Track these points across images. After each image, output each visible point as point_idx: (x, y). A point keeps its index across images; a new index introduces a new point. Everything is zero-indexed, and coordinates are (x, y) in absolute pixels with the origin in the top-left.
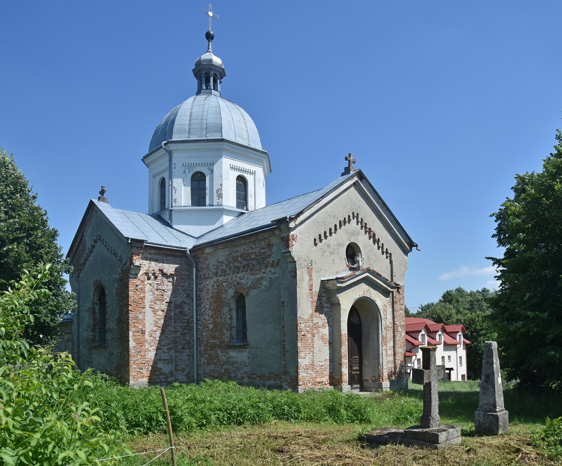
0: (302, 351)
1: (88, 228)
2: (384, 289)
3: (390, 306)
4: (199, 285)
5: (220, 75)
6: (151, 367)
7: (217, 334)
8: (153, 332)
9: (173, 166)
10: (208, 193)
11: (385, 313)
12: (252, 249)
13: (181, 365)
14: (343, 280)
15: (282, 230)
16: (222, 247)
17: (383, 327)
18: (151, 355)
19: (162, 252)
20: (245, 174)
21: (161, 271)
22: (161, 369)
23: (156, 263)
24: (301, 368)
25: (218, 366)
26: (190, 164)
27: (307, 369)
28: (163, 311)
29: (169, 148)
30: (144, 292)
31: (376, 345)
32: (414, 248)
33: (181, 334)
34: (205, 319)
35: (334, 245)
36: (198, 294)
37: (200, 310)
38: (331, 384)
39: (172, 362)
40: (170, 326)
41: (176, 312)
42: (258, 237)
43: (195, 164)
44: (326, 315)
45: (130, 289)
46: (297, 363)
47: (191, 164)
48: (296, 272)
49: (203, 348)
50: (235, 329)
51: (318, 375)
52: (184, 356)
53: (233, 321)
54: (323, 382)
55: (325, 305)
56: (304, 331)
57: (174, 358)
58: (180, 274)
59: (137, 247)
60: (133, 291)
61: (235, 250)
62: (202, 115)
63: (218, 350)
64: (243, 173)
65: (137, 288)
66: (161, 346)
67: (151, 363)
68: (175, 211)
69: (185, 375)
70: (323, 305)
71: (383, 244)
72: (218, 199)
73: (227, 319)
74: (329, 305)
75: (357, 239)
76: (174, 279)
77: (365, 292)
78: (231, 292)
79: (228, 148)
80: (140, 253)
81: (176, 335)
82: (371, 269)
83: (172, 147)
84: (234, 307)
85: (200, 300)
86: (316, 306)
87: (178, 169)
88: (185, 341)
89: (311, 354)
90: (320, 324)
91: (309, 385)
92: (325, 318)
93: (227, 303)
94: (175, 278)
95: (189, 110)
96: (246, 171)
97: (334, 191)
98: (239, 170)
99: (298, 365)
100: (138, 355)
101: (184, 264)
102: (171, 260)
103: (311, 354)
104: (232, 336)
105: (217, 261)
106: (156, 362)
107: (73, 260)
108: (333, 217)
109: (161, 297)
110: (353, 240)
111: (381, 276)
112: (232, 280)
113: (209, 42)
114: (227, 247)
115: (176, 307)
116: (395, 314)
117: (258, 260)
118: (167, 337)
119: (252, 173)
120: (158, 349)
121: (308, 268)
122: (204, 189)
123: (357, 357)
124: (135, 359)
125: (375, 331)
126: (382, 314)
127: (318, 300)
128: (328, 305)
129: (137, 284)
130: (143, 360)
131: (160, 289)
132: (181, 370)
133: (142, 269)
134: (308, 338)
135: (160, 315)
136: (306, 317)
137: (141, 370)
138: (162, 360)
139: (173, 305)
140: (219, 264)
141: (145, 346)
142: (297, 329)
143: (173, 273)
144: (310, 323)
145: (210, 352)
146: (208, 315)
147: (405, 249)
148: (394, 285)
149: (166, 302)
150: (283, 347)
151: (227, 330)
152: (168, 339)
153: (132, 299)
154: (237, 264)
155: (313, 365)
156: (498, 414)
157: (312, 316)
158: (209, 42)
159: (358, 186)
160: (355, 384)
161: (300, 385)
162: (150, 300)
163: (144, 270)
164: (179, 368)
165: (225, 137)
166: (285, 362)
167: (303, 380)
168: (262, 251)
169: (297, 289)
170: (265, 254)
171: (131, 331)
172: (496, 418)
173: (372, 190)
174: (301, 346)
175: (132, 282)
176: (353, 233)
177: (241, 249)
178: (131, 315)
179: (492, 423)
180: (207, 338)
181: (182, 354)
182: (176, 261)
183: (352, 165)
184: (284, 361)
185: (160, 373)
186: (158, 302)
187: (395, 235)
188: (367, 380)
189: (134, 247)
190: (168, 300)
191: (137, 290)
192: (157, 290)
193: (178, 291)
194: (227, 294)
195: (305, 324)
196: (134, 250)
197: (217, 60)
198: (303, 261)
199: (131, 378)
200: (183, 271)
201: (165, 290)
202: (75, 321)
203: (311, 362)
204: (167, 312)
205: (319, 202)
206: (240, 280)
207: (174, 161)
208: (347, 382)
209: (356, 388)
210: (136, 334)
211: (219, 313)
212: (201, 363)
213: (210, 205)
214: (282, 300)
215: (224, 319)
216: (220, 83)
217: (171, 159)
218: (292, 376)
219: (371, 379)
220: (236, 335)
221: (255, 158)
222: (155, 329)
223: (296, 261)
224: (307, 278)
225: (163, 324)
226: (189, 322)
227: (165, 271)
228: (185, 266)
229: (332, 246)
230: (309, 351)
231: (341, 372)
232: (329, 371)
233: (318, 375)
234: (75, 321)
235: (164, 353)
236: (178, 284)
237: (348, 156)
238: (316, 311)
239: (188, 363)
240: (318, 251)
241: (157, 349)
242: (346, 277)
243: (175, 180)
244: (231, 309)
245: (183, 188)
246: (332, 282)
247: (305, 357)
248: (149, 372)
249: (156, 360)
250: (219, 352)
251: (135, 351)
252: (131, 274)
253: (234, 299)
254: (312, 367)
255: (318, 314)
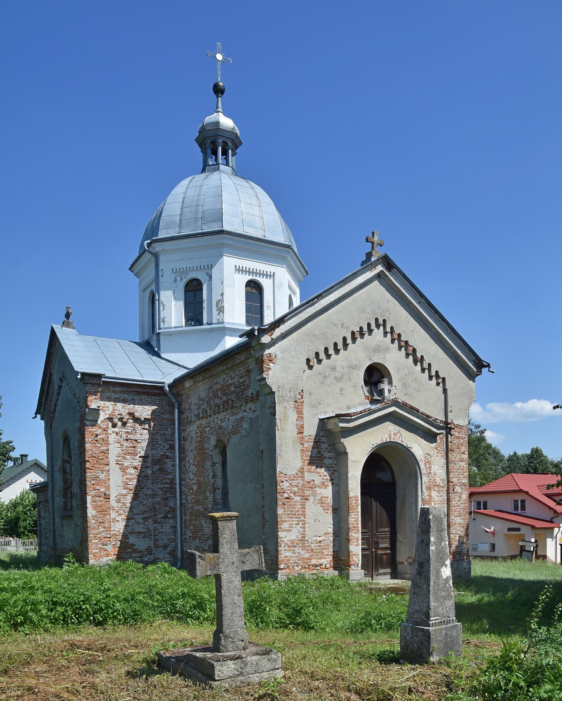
0: (285, 521)
1: (55, 364)
2: (426, 430)
3: (442, 456)
4: (183, 432)
5: (232, 143)
6: (119, 543)
7: (201, 497)
8: (122, 497)
9: (160, 274)
10: (206, 307)
11: (428, 466)
12: (232, 378)
13: (162, 540)
14: (350, 418)
15: (255, 348)
16: (201, 379)
17: (424, 486)
18: (119, 527)
19: (131, 390)
20: (260, 277)
21: (131, 414)
22: (134, 545)
23: (123, 404)
24: (283, 545)
25: (202, 541)
26: (181, 270)
27: (294, 546)
28: (135, 468)
29: (154, 249)
30: (106, 442)
31: (414, 513)
32: (485, 370)
33: (161, 498)
34: (189, 478)
35: (343, 367)
36: (182, 445)
37: (185, 466)
38: (335, 568)
39: (149, 535)
40: (146, 488)
41: (155, 469)
42: (235, 361)
43: (188, 269)
44: (328, 469)
45: (86, 440)
46: (276, 537)
47: (183, 268)
48: (275, 408)
49: (188, 517)
50: (221, 490)
51: (313, 555)
52: (167, 528)
53: (217, 480)
54: (321, 565)
55: (327, 455)
56: (289, 492)
57: (153, 531)
58: (159, 418)
59: (93, 384)
60: (91, 443)
61: (215, 381)
62: (198, 200)
63: (202, 520)
64: (256, 276)
65: (96, 439)
66: (133, 514)
67: (120, 537)
68: (164, 335)
69: (168, 553)
70: (323, 455)
71: (429, 365)
72: (219, 314)
73: (210, 477)
74: (333, 454)
75: (384, 358)
76: (150, 425)
77: (392, 434)
78: (213, 440)
79: (230, 242)
80: (97, 392)
81: (155, 500)
82: (399, 400)
83: (157, 247)
84: (218, 461)
85: (184, 452)
86: (311, 456)
87: (166, 278)
88: (168, 509)
89: (301, 525)
90: (317, 482)
91: (297, 569)
92: (326, 473)
93: (210, 455)
94: (152, 424)
95: (182, 195)
96: (260, 274)
97: (341, 287)
98: (249, 272)
99: (278, 540)
100: (100, 527)
101: (165, 405)
102: (146, 400)
103: (301, 525)
104: (216, 501)
105: (199, 398)
106: (127, 536)
107: (46, 406)
108: (340, 326)
109: (131, 450)
110: (377, 359)
111: (418, 411)
112: (214, 423)
113: (218, 97)
114: (206, 378)
115: (155, 462)
116: (450, 468)
117: (237, 393)
118: (142, 502)
119: (270, 276)
120: (128, 519)
121: (295, 401)
122: (201, 302)
123: (387, 529)
124: (96, 531)
125: (413, 492)
126: (422, 466)
127: (313, 448)
128: (331, 454)
129: (97, 433)
130: (107, 534)
131: (131, 440)
132: (162, 547)
133: (101, 413)
134: (296, 502)
135: (132, 474)
136: (292, 472)
137: (105, 547)
138: (136, 533)
139: (149, 460)
140: (201, 403)
141: (110, 515)
142: (277, 490)
143: (149, 417)
144: (299, 480)
145: (195, 522)
146: (192, 472)
147: (470, 371)
148: (441, 425)
149: (140, 457)
150: (263, 515)
151: (210, 492)
152: (143, 505)
153: (90, 453)
154: (217, 401)
155: (303, 540)
156: (430, 629)
157: (302, 470)
158: (218, 97)
159: (386, 279)
160: (382, 568)
161: (281, 569)
162: (116, 454)
163: (107, 414)
164: (160, 543)
165: (226, 228)
166: (264, 536)
167: (286, 562)
168: (241, 380)
169: (277, 432)
170: (244, 385)
171: (89, 495)
172: (427, 635)
173: (408, 283)
174: (282, 514)
175: (90, 431)
176: (377, 349)
177: (220, 380)
178: (89, 474)
179: (421, 643)
180: (192, 503)
181: (164, 525)
182: (152, 401)
183: (377, 248)
184: (264, 535)
185: (133, 550)
186: (127, 457)
187: (452, 351)
188: (402, 563)
189: (88, 383)
190: (143, 453)
191: (97, 441)
192: (127, 440)
193: (156, 442)
194: (209, 443)
195: (290, 482)
196: (88, 388)
197: (226, 122)
198: (287, 392)
199: (91, 556)
200: (165, 414)
201: (139, 441)
202: (50, 486)
203: (300, 536)
204: (141, 469)
205: (313, 304)
206: (222, 422)
207: (161, 266)
208: (360, 566)
209: (385, 574)
210: (96, 499)
211: (202, 470)
212: (187, 537)
213: (208, 324)
214: (261, 448)
215: (207, 477)
216: (233, 155)
217: (158, 264)
218: (272, 557)
219: (407, 561)
220: (222, 498)
221: (274, 254)
222: (124, 492)
223: (274, 392)
224: (293, 416)
225: (136, 486)
226: (172, 481)
227: (137, 415)
228: (166, 408)
229: (339, 369)
230: (297, 521)
231: (349, 551)
232: (332, 550)
233: (313, 555)
234: (50, 486)
235: (138, 524)
236: (157, 432)
237: (371, 236)
238: (310, 464)
239: (172, 537)
240: (314, 377)
241: (127, 519)
242: (354, 414)
243: (162, 293)
244: (213, 463)
245: (173, 303)
246: (333, 421)
247: (290, 529)
248: (117, 549)
249: (127, 533)
250: (203, 522)
251: (96, 522)
252: (87, 420)
253: (217, 450)
254: (302, 543)
255: (313, 468)
